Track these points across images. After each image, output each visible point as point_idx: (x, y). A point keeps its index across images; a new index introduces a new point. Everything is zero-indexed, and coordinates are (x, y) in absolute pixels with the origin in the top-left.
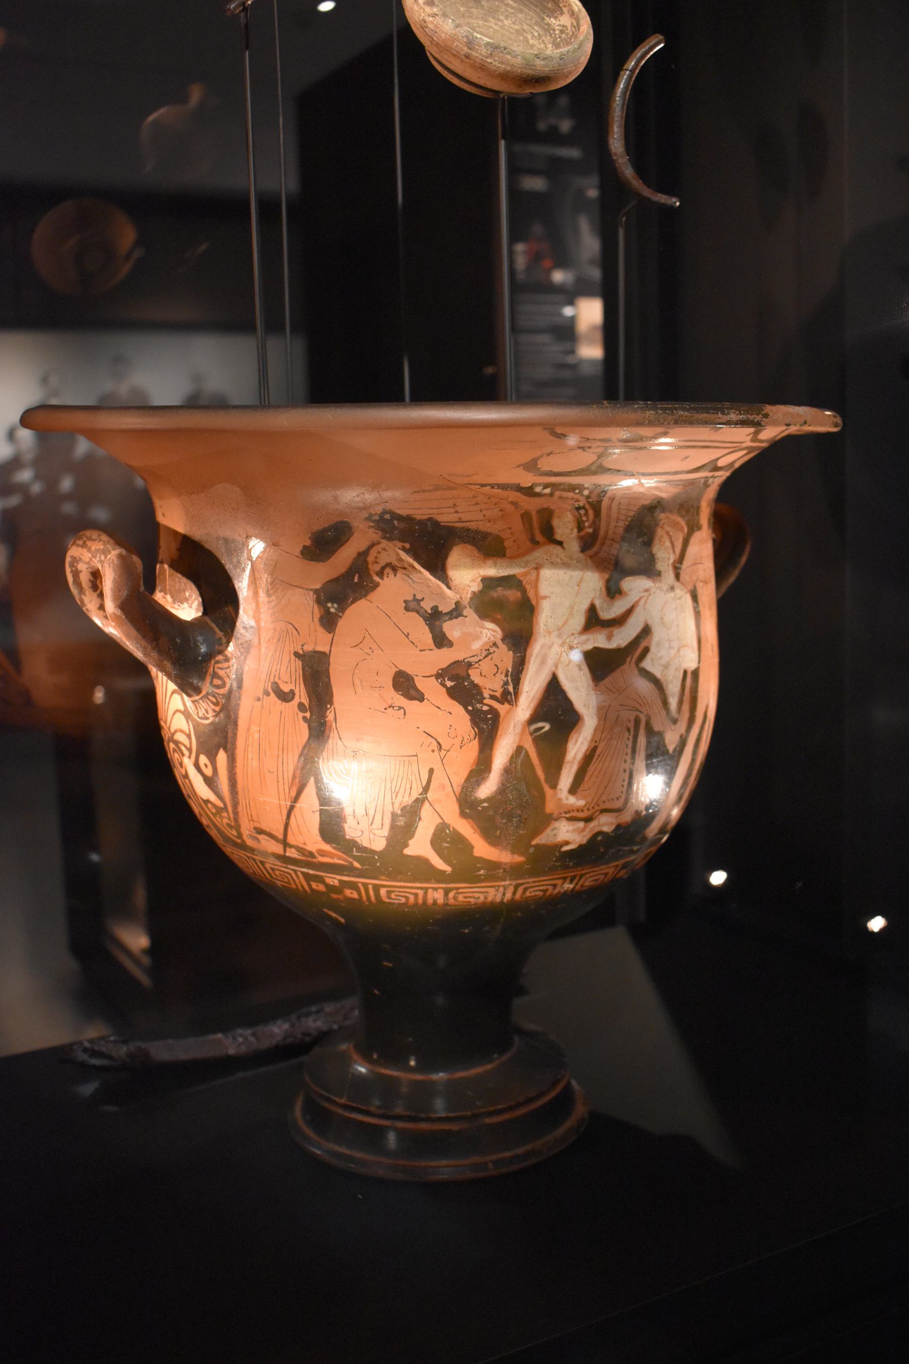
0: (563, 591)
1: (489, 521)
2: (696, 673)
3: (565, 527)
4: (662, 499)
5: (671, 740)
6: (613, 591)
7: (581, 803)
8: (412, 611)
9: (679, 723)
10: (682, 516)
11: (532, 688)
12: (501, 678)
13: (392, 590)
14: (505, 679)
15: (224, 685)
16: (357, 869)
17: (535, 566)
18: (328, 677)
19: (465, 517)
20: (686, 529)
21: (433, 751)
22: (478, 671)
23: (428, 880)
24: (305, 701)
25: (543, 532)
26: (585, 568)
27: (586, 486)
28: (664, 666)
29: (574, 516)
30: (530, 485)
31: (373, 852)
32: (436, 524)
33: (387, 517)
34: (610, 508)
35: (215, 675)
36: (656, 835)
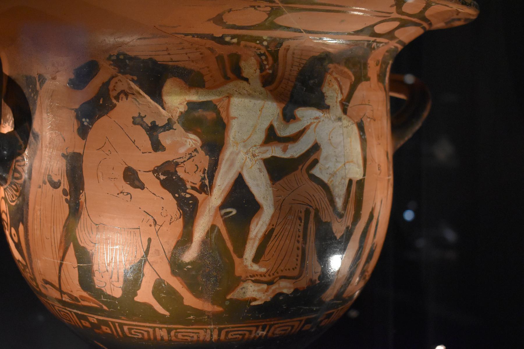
0: (249, 115)
1: (193, 61)
2: (361, 183)
3: (250, 68)
4: (329, 53)
5: (338, 229)
6: (288, 117)
7: (263, 270)
8: (138, 124)
9: (344, 218)
10: (348, 68)
11: (223, 183)
12: (200, 174)
13: (125, 109)
14: (203, 175)
15: (20, 178)
16: (105, 311)
17: (227, 95)
18: (82, 171)
19: (175, 58)
20: (353, 78)
21: (151, 225)
22: (183, 169)
23: (154, 322)
24: (67, 188)
25: (232, 71)
26: (266, 98)
27: (265, 38)
28: (330, 174)
29: (257, 60)
30: (221, 35)
31: (114, 298)
32: (155, 62)
33: (122, 57)
34: (285, 56)
35: (16, 170)
36: (333, 300)
